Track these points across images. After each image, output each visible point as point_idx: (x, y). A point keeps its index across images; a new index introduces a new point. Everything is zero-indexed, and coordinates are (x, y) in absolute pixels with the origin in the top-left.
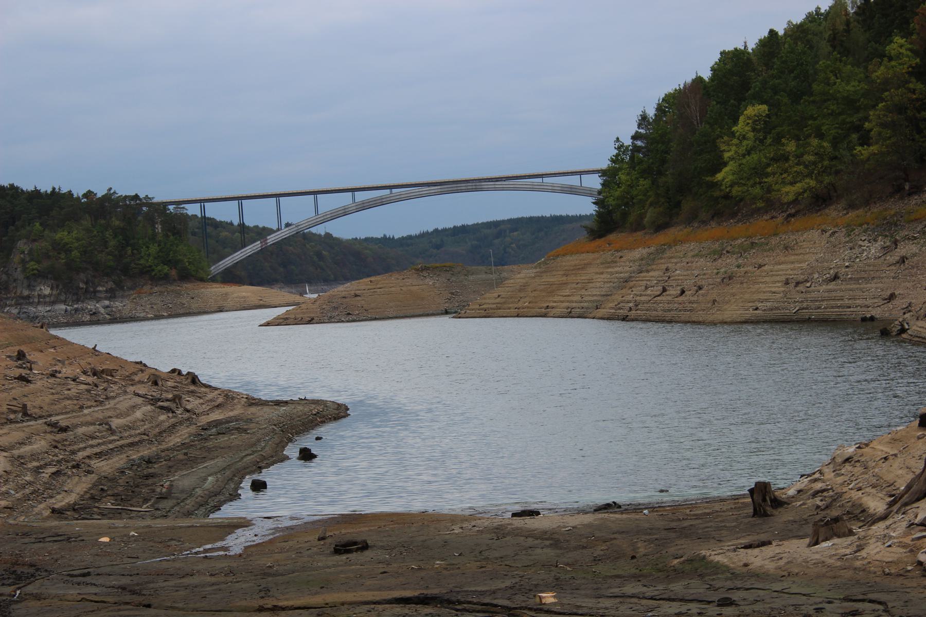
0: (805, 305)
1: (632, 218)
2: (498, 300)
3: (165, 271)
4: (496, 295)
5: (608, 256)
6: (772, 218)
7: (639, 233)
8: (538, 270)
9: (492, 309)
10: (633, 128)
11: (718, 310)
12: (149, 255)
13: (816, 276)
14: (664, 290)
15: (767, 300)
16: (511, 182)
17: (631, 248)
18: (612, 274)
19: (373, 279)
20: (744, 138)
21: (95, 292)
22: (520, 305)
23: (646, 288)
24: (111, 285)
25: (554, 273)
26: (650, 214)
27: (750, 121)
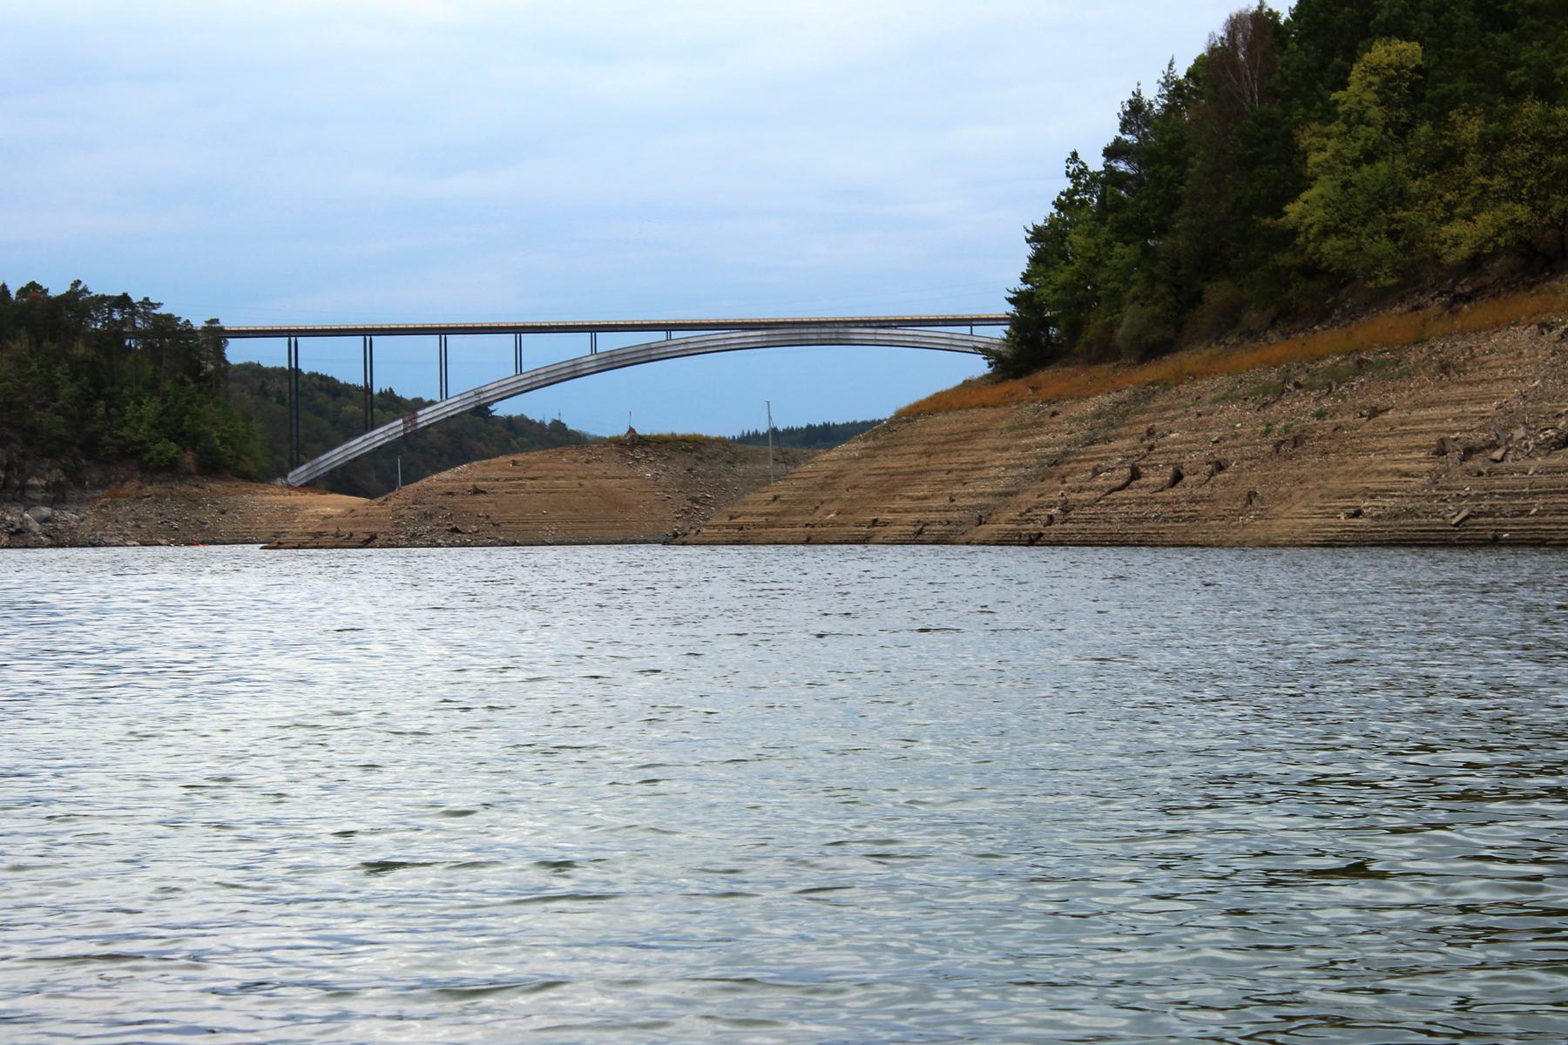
0: (1485, 505)
1: (1090, 333)
2: (770, 508)
3: (171, 454)
4: (769, 496)
5: (1027, 412)
6: (1416, 308)
7: (1106, 367)
8: (870, 443)
9: (755, 526)
10: (1109, 130)
11: (1258, 517)
12: (140, 419)
13: (1519, 433)
14: (1135, 474)
15: (1384, 493)
16: (909, 331)
17: (1082, 396)
18: (1028, 447)
19: (519, 458)
20: (1362, 119)
21: (24, 488)
22: (817, 517)
23: (1096, 472)
24: (56, 475)
25: (903, 450)
26: (1131, 319)
27: (1376, 79)
